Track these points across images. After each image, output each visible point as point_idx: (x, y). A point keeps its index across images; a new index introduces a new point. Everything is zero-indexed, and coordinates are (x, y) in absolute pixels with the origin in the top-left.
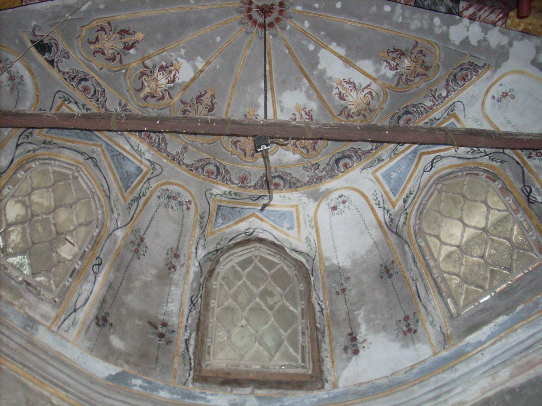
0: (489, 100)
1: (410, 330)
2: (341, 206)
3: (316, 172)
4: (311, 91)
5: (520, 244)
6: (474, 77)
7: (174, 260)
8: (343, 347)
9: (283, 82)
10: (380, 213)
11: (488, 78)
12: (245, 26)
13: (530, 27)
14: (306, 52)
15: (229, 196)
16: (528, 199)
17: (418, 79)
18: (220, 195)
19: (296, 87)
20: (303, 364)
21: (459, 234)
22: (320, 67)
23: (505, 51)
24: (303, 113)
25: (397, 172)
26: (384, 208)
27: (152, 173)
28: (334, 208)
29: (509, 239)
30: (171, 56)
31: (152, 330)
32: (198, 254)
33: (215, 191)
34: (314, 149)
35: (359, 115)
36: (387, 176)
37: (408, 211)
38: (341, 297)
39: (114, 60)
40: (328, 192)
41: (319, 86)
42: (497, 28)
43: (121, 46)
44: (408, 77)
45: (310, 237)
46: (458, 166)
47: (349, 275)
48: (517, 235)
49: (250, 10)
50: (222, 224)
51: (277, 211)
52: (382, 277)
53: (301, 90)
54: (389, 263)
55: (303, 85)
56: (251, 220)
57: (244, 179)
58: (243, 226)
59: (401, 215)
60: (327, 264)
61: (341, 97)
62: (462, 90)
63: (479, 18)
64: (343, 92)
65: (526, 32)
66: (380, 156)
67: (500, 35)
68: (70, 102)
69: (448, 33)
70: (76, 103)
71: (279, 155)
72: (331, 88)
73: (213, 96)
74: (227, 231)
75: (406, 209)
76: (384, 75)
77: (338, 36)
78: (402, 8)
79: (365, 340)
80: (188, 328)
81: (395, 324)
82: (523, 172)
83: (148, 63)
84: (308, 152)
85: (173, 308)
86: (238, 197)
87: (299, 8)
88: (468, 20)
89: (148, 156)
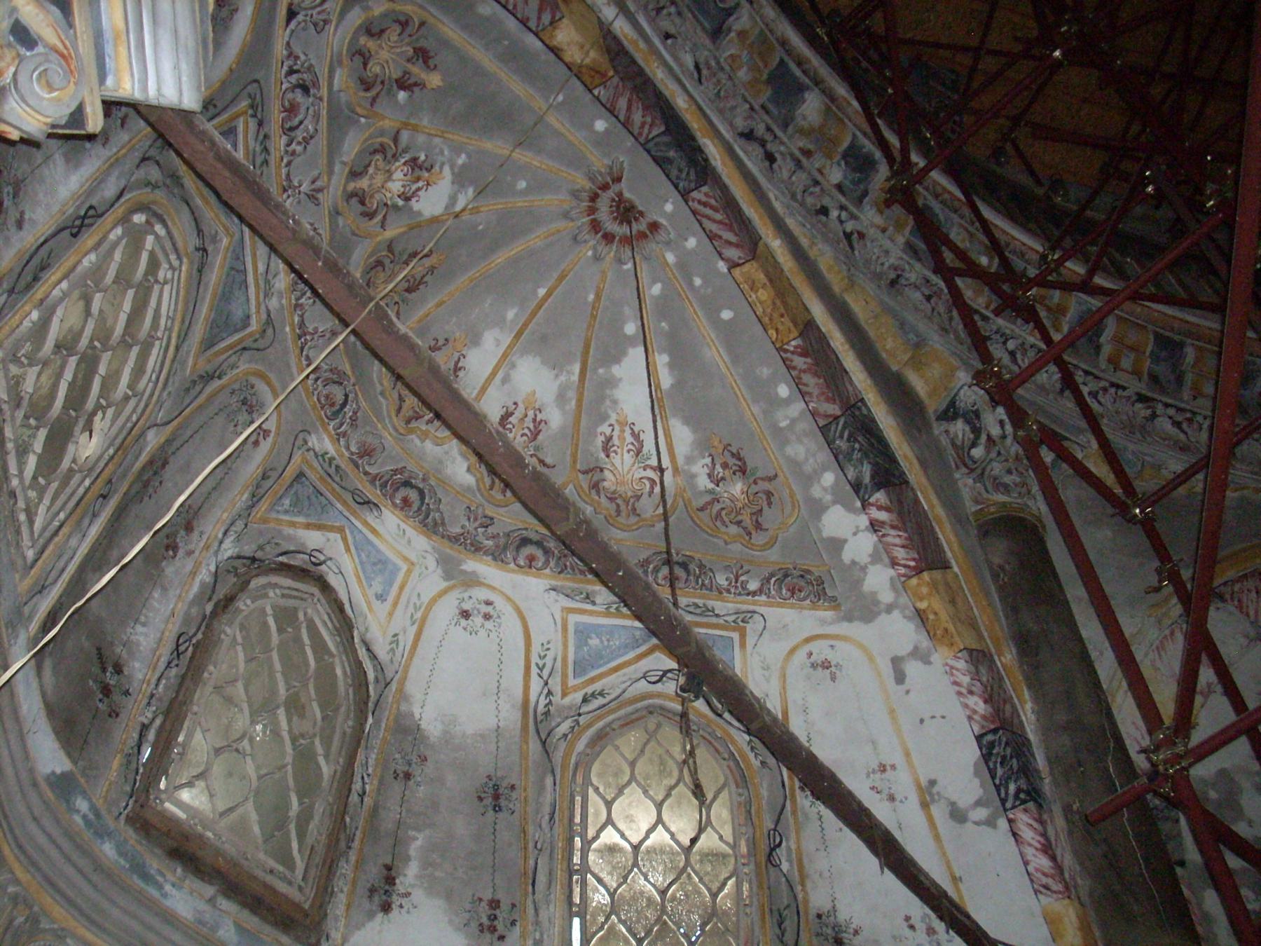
0: (801, 655)
1: (493, 929)
2: (478, 620)
4: (572, 394)
5: (725, 913)
6: (808, 602)
7: (183, 533)
8: (369, 885)
9: (544, 339)
10: (536, 685)
11: (823, 622)
12: (574, 203)
13: (931, 617)
14: (616, 325)
15: (326, 466)
16: (770, 854)
17: (733, 529)
18: (316, 454)
19: (557, 366)
20: (302, 884)
21: (645, 827)
22: (616, 370)
23: (876, 609)
24: (531, 413)
25: (602, 642)
26: (546, 684)
27: (256, 340)
28: (466, 614)
29: (714, 896)
30: (442, 153)
31: (96, 670)
32: (224, 546)
33: (313, 441)
35: (611, 499)
36: (583, 633)
37: (582, 720)
38: (397, 787)
39: (367, 90)
40: (472, 581)
41: (591, 399)
42: (891, 572)
43: (396, 74)
44: (723, 513)
47: (428, 753)
48: (726, 896)
49: (605, 187)
50: (286, 512)
51: (378, 551)
52: (481, 799)
53: (557, 376)
54: (504, 784)
55: (568, 372)
56: (332, 535)
57: (367, 452)
58: (313, 539)
59: (567, 718)
60: (403, 708)
61: (607, 447)
62: (779, 605)
63: (884, 536)
64: (616, 441)
65: (921, 616)
66: (594, 592)
67: (888, 585)
68: (254, 116)
69: (828, 508)
70: (260, 124)
71: (447, 453)
72: (604, 418)
73: (432, 270)
75: (580, 715)
76: (693, 476)
77: (683, 357)
78: (802, 413)
79: (408, 895)
80: (154, 701)
81: (470, 900)
82: (784, 806)
83: (405, 136)
85: (141, 639)
86: (337, 479)
87: (670, 258)
88: (867, 523)
89: (273, 303)
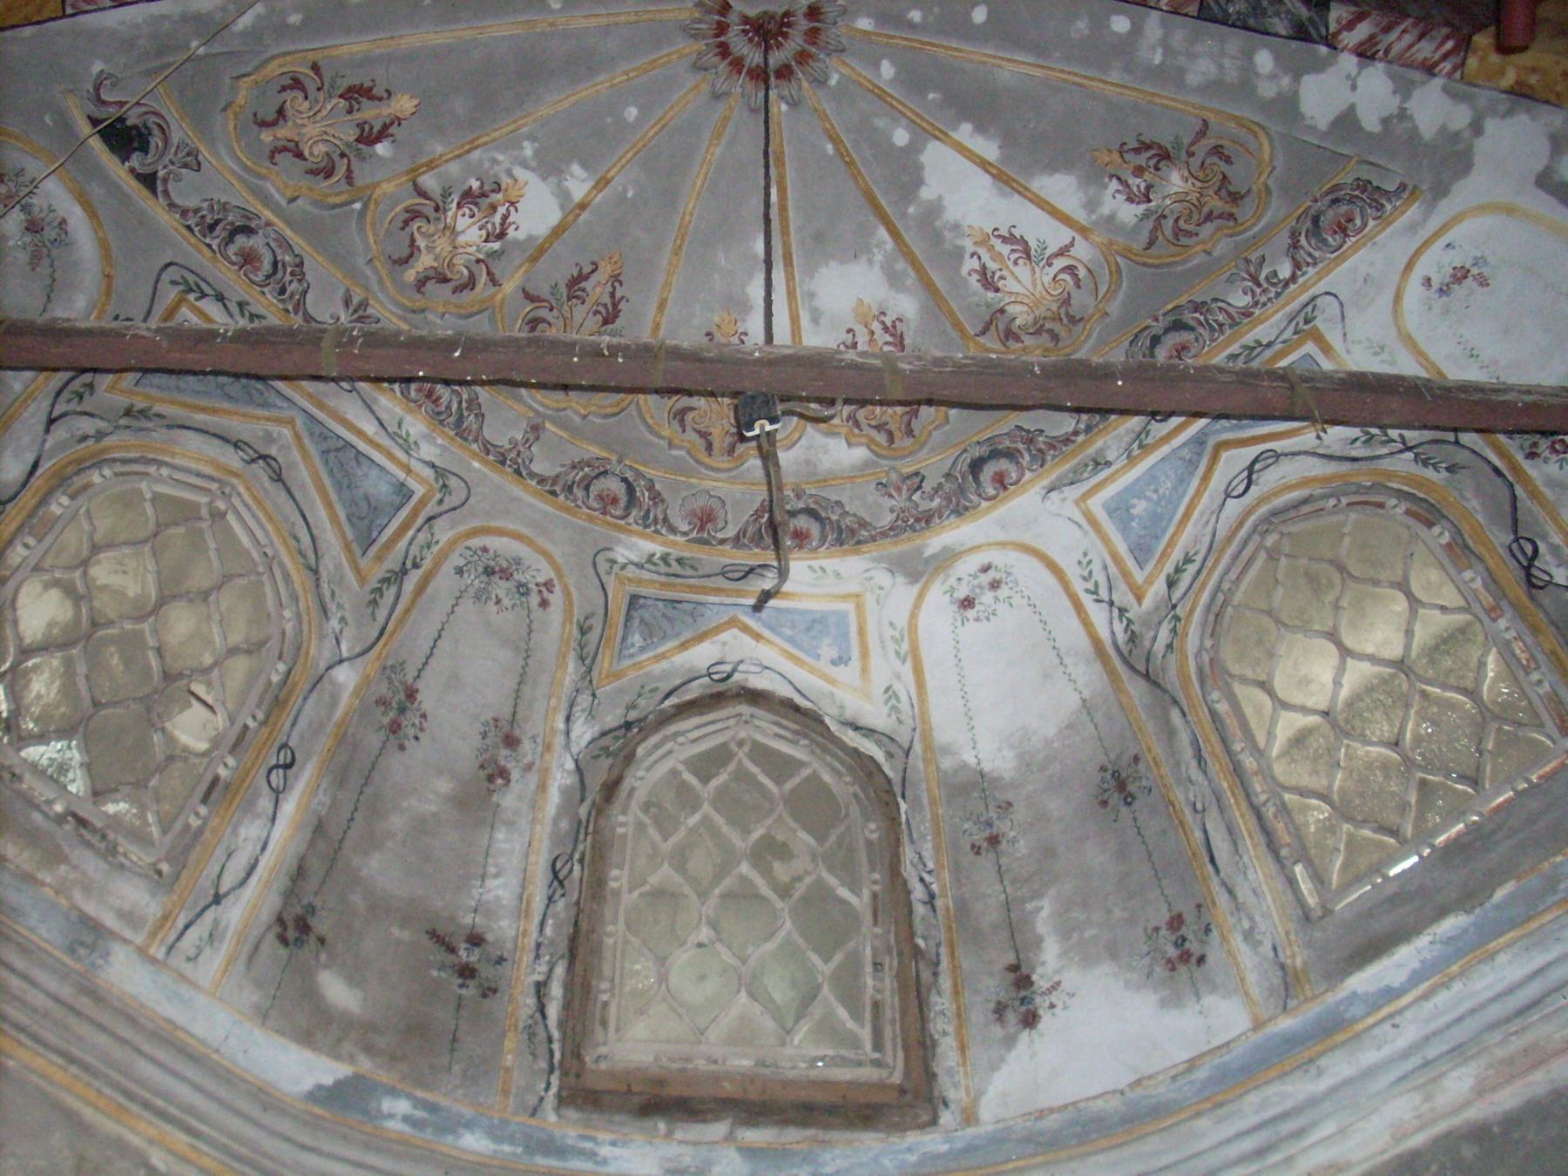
0: (1414, 289)
1: (1185, 957)
2: (987, 597)
3: (916, 497)
4: (901, 265)
5: (1504, 706)
6: (1371, 223)
7: (504, 752)
8: (992, 1005)
9: (819, 237)
10: (1099, 616)
11: (1413, 227)
12: (710, 76)
13: (1533, 79)
14: (886, 151)
15: (663, 568)
16: (1529, 575)
17: (1208, 229)
18: (636, 565)
19: (858, 251)
20: (877, 1055)
21: (1327, 677)
22: (926, 194)
23: (1461, 146)
24: (876, 326)
25: (1149, 499)
26: (1111, 603)
27: (441, 501)
28: (967, 603)
29: (1472, 693)
30: (494, 161)
31: (440, 955)
32: (573, 735)
33: (622, 554)
34: (910, 432)
35: (1038, 332)
36: (1119, 509)
37: (1179, 611)
38: (986, 861)
39: (329, 175)
40: (949, 557)
41: (923, 251)
42: (1438, 82)
43: (351, 134)
44: (1181, 223)
45: (897, 687)
46: (1325, 480)
47: (1010, 795)
48: (1495, 681)
49: (722, 29)
50: (642, 649)
51: (802, 613)
52: (1104, 803)
53: (870, 261)
54: (1125, 760)
55: (878, 246)
56: (725, 636)
57: (705, 519)
58: (702, 655)
59: (1160, 623)
60: (946, 763)
61: (987, 280)
62: (1337, 262)
63: (1387, 52)
64: (992, 266)
65: (1521, 94)
66: (1101, 451)
67: (1448, 101)
68: (204, 295)
69: (1296, 94)
70: (220, 298)
71: (808, 448)
72: (958, 255)
73: (616, 279)
74: (657, 668)
75: (1174, 607)
76: (1111, 218)
77: (978, 105)
78: (1163, 24)
79: (1056, 986)
80: (543, 950)
81: (1144, 938)
82: (1514, 498)
83: (429, 181)
84: (891, 439)
85: (500, 892)
86: (689, 572)
87: (864, 23)
88: (1354, 59)
89: (428, 451)
